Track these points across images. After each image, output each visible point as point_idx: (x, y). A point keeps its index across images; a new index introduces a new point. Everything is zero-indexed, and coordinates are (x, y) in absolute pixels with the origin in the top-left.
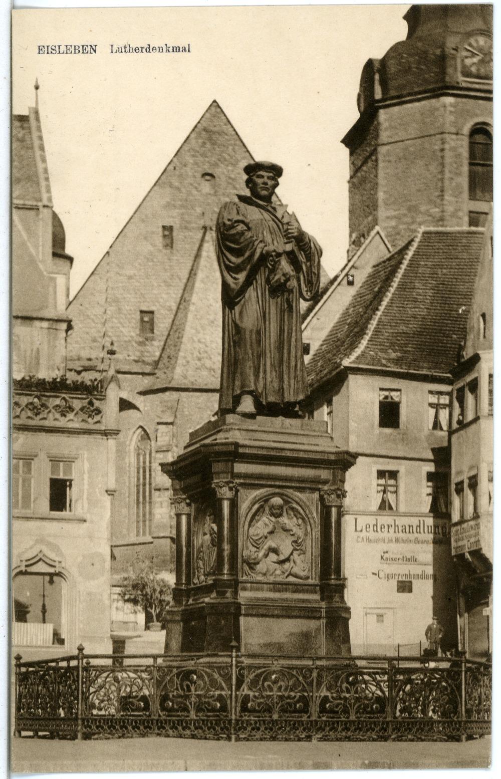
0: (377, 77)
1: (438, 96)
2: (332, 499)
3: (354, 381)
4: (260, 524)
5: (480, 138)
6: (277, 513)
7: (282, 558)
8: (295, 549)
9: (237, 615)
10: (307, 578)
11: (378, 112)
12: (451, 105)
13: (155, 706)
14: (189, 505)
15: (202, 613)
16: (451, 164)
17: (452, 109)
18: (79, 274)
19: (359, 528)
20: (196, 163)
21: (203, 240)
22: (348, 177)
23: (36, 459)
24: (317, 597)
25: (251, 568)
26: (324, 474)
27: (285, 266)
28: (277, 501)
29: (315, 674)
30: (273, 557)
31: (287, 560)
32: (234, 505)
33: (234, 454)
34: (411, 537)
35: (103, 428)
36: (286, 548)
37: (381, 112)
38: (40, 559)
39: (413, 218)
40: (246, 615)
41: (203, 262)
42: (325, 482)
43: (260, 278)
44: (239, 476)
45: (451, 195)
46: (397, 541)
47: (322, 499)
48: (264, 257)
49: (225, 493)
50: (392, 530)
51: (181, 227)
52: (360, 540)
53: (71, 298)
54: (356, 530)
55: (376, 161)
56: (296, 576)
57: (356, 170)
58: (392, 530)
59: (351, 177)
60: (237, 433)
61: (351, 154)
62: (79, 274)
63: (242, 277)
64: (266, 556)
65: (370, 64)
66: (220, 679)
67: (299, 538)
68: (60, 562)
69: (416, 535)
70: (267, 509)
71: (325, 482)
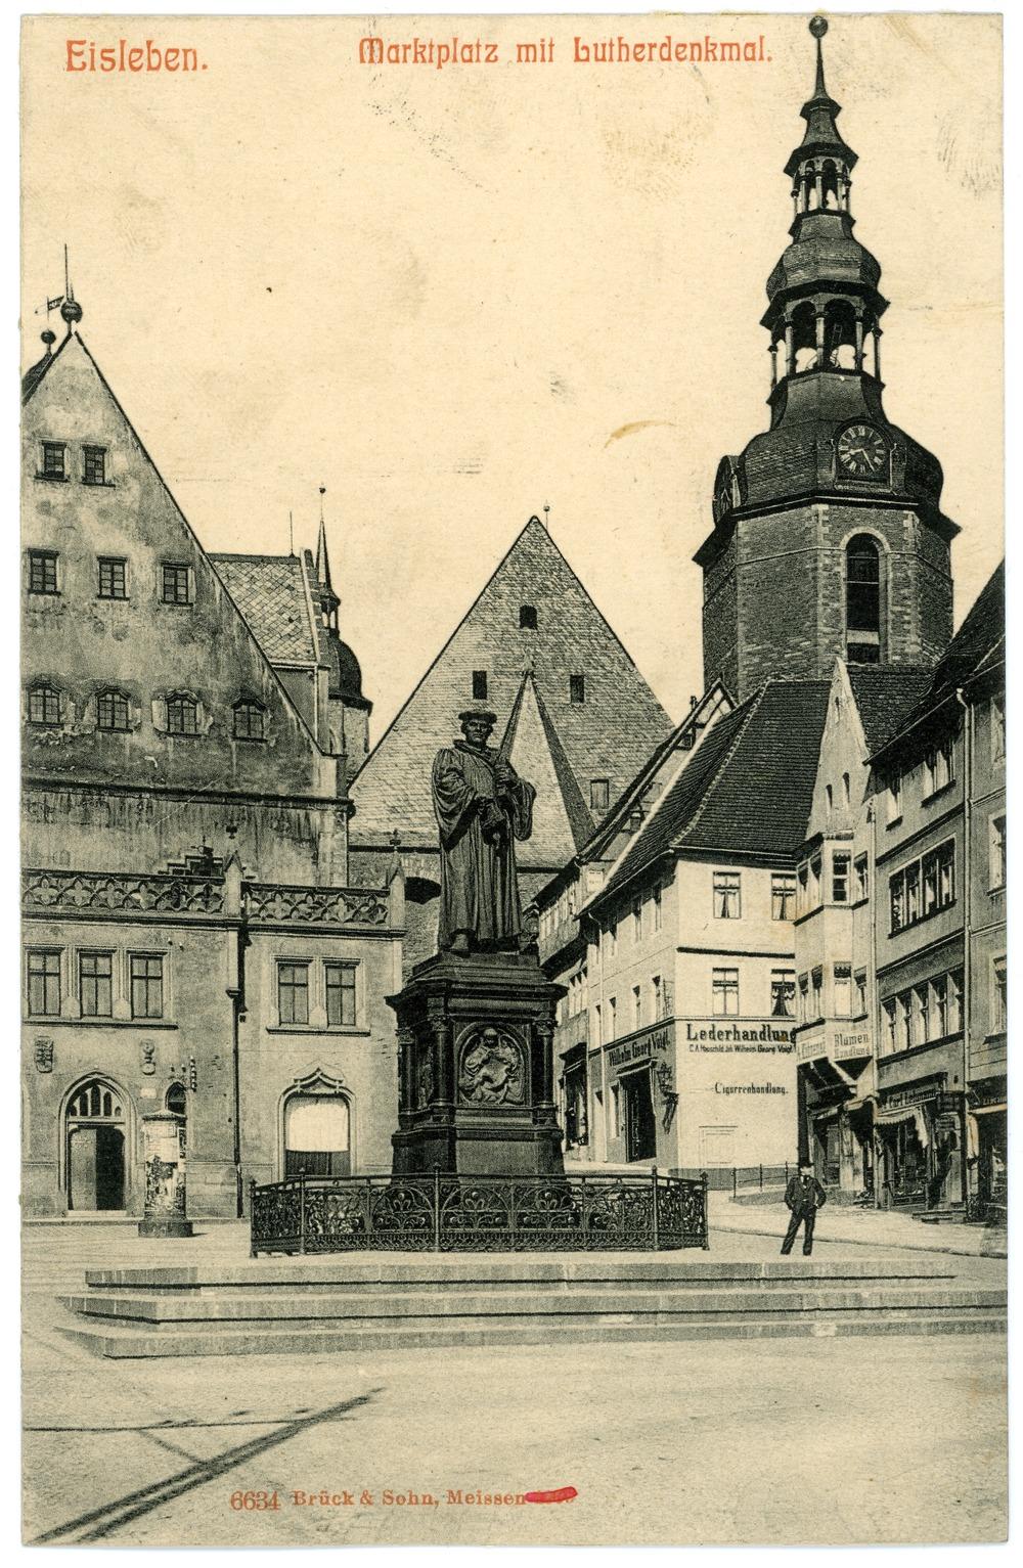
0: (734, 481)
1: (808, 504)
2: (543, 1031)
3: (684, 869)
4: (476, 1053)
5: (862, 555)
6: (493, 1042)
7: (496, 1084)
8: (509, 1077)
9: (453, 1138)
10: (521, 1103)
11: (736, 523)
12: (825, 513)
13: (368, 1223)
14: (412, 1036)
15: (422, 1142)
16: (825, 587)
17: (826, 518)
18: (379, 722)
19: (693, 1036)
20: (512, 594)
21: (522, 688)
22: (702, 604)
23: (310, 965)
24: (529, 1121)
25: (467, 1096)
26: (536, 1006)
27: (494, 809)
28: (490, 1032)
29: (512, 1191)
30: (487, 1084)
31: (502, 1087)
32: (449, 1041)
33: (448, 990)
34: (755, 1044)
35: (387, 928)
36: (500, 1075)
37: (740, 523)
38: (319, 1079)
39: (779, 652)
40: (462, 1139)
41: (523, 713)
42: (537, 1014)
43: (476, 824)
44: (455, 1010)
45: (826, 625)
46: (737, 1048)
47: (534, 1030)
48: (476, 804)
49: (441, 1028)
50: (731, 1037)
51: (495, 673)
52: (694, 1048)
53: (372, 746)
54: (689, 1038)
55: (735, 584)
56: (512, 1102)
57: (711, 592)
58: (731, 1037)
59: (706, 604)
60: (462, 970)
61: (706, 573)
62: (379, 722)
63: (455, 822)
64: (482, 1083)
65: (725, 461)
66: (425, 1198)
67: (512, 1065)
68: (340, 1082)
69: (760, 1042)
70: (482, 1039)
71: (537, 1014)
